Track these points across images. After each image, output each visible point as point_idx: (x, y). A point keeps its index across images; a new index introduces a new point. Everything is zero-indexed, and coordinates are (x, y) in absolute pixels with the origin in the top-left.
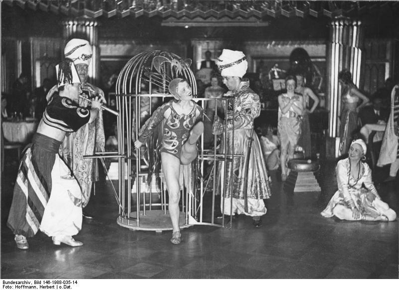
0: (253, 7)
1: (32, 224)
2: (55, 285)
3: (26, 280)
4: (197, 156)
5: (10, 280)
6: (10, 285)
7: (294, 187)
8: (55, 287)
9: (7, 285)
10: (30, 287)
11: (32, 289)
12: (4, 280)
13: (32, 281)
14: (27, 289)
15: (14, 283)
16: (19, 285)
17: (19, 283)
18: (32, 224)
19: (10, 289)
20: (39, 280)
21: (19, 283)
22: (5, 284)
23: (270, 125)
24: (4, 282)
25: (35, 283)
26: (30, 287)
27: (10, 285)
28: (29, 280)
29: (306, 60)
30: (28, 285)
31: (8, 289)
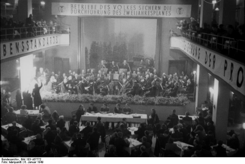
0: (88, 90)
1: (136, 115)
2: (22, 161)
3: (16, 158)
4: (140, 104)
5: (6, 158)
6: (6, 161)
7: (30, 136)
8: (22, 162)
9: (4, 161)
10: (18, 162)
11: (32, 163)
12: (2, 158)
13: (20, 158)
14: (32, 163)
15: (9, 159)
16: (12, 161)
17: (12, 160)
18: (136, 115)
19: (6, 163)
20: (24, 158)
21: (12, 160)
22: (3, 160)
23: (63, 118)
24: (2, 159)
25: (22, 159)
26: (18, 162)
27: (6, 161)
28: (18, 158)
29: (20, 120)
30: (17, 161)
31: (5, 163)
